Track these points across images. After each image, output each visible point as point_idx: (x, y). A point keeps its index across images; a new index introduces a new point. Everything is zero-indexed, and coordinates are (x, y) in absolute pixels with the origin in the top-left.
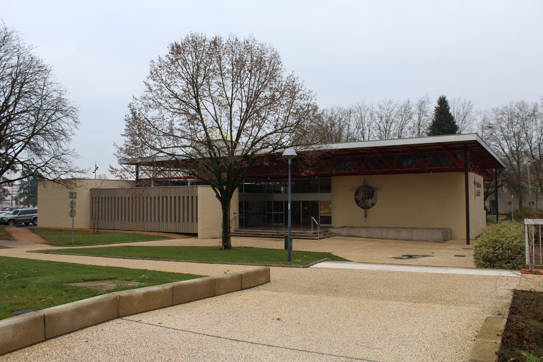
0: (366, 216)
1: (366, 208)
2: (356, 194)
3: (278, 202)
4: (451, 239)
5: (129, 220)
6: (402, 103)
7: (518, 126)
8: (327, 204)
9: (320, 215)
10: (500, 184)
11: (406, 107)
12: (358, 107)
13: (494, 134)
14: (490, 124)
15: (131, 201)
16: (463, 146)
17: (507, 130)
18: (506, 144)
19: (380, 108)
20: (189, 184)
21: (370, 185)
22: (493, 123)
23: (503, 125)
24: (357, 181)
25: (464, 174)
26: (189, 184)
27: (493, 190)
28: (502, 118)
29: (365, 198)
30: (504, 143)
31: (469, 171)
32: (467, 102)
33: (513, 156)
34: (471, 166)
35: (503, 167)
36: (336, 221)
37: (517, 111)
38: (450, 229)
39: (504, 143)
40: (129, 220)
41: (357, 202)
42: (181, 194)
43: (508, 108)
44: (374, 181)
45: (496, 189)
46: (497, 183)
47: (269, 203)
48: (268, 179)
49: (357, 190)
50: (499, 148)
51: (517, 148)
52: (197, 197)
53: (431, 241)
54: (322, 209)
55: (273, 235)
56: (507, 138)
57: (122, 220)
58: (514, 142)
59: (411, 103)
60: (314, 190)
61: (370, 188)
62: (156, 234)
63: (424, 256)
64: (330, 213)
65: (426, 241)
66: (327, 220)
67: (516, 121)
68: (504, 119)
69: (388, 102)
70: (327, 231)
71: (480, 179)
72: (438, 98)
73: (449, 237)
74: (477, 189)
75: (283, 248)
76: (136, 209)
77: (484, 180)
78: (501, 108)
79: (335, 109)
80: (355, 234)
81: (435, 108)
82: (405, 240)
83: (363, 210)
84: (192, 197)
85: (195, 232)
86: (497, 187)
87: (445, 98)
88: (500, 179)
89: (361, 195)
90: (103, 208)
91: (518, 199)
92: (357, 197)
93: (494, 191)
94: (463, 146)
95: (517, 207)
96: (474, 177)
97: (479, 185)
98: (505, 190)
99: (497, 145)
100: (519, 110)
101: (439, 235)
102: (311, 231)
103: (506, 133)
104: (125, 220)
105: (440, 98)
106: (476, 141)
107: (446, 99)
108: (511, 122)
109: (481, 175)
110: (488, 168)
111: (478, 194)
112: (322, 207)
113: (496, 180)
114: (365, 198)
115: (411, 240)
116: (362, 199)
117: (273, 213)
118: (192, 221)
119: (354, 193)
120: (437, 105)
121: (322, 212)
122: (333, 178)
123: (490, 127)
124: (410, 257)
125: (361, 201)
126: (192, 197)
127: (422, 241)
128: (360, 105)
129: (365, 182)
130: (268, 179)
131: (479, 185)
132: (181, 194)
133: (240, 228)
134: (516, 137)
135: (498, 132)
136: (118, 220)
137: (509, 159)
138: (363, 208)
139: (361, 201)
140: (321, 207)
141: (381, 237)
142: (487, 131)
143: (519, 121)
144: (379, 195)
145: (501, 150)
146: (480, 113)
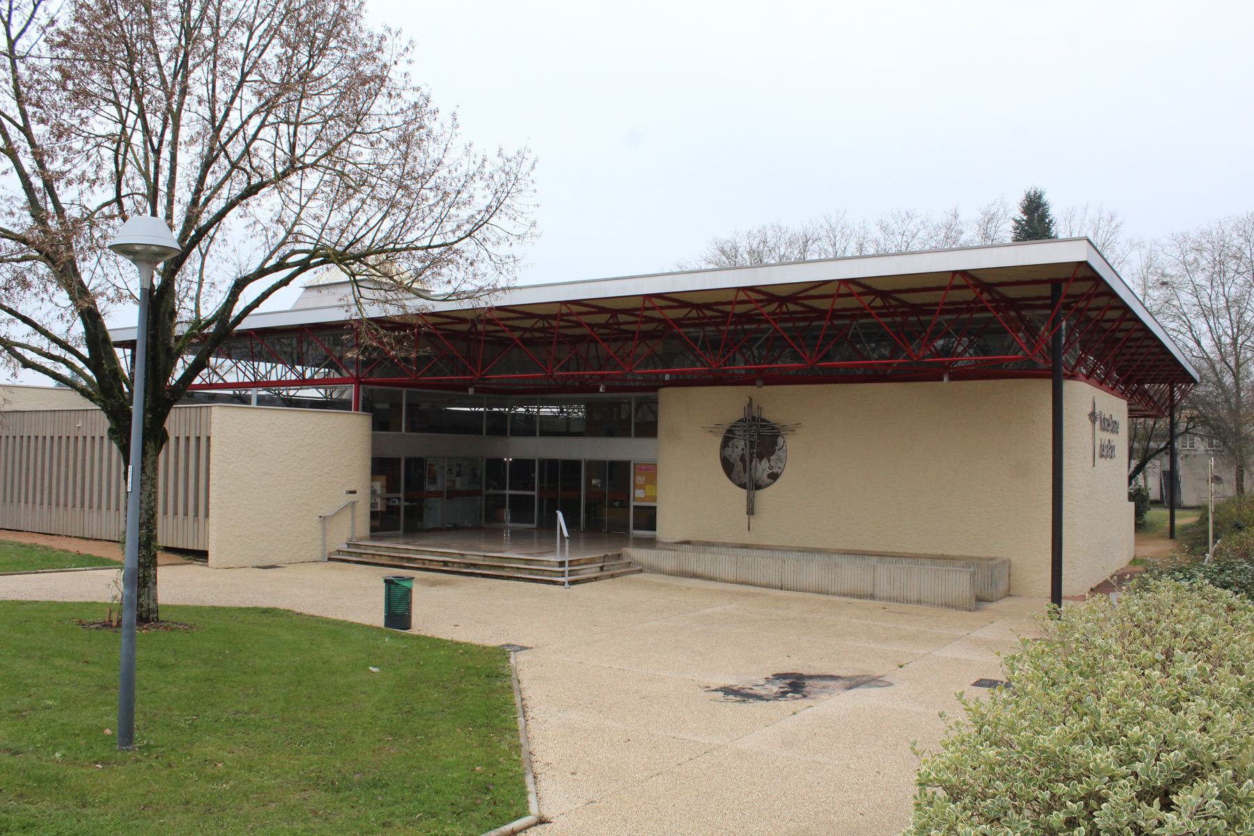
0: (751, 511)
1: (755, 486)
2: (725, 444)
3: (604, 462)
4: (1009, 594)
5: (50, 504)
6: (939, 217)
7: (1240, 280)
8: (650, 470)
9: (632, 503)
10: (1182, 427)
11: (949, 228)
12: (826, 226)
13: (1175, 302)
14: (1163, 275)
15: (32, 444)
16: (1045, 290)
17: (1209, 291)
18: (1205, 327)
19: (884, 229)
20: (254, 400)
21: (764, 416)
22: (1173, 273)
23: (1200, 278)
24: (728, 403)
25: (1048, 384)
26: (254, 400)
27: (1163, 445)
28: (1196, 260)
29: (751, 455)
30: (1201, 326)
31: (1073, 377)
32: (1106, 216)
33: (1223, 360)
34: (1080, 361)
35: (1193, 380)
36: (667, 528)
37: (1238, 241)
38: (1007, 563)
39: (1201, 326)
40: (50, 504)
41: (728, 466)
42: (182, 430)
43: (1214, 233)
44: (778, 403)
45: (1171, 443)
46: (1173, 424)
47: (495, 465)
48: (471, 391)
49: (730, 431)
50: (1187, 336)
51: (1235, 340)
52: (209, 438)
53: (933, 604)
54: (642, 487)
55: (445, 563)
56: (1208, 313)
57: (34, 503)
58: (1227, 323)
59: (961, 218)
60: (618, 429)
61: (765, 424)
62: (74, 546)
63: (854, 683)
64: (654, 499)
65: (919, 602)
66: (648, 518)
67: (1235, 267)
68: (1203, 263)
69: (904, 216)
70: (619, 556)
71: (1116, 407)
72: (1021, 197)
73: (1002, 588)
74: (1106, 436)
75: (379, 619)
76: (67, 472)
77: (1132, 414)
78: (1194, 235)
79: (770, 234)
80: (700, 571)
81: (1013, 223)
82: (852, 595)
83: (743, 492)
84: (198, 439)
85: (201, 548)
86: (1172, 436)
87: (1040, 197)
88: (1182, 417)
89: (739, 446)
90: (71, 463)
91: (1234, 470)
92: (728, 451)
93: (1165, 448)
94: (1045, 290)
95: (1229, 490)
96: (1083, 397)
97: (1110, 425)
98: (1200, 446)
99: (1182, 330)
100: (1242, 240)
101: (960, 584)
102: (553, 552)
103: (1206, 300)
104: (42, 504)
105: (1028, 196)
106: (1085, 264)
107: (1045, 198)
108: (1219, 272)
109: (1122, 395)
110: (1152, 382)
111: (1107, 451)
112: (640, 479)
113: (1171, 416)
114: (751, 455)
115: (872, 597)
116: (742, 459)
117: (508, 492)
118: (196, 515)
119: (718, 441)
120: (1019, 215)
121: (640, 493)
122: (664, 393)
123: (1164, 284)
124: (795, 684)
125: (739, 466)
126: (198, 439)
127: (907, 601)
128: (833, 221)
129: (750, 405)
130: (471, 391)
131: (1110, 425)
132: (182, 430)
133: (372, 538)
134: (1232, 310)
135: (1186, 297)
136: (26, 502)
137: (1213, 367)
138: (742, 486)
139: (739, 466)
140: (636, 479)
141: (778, 583)
142: (1155, 293)
143: (1241, 269)
144: (791, 445)
145: (1192, 344)
146: (1140, 245)
